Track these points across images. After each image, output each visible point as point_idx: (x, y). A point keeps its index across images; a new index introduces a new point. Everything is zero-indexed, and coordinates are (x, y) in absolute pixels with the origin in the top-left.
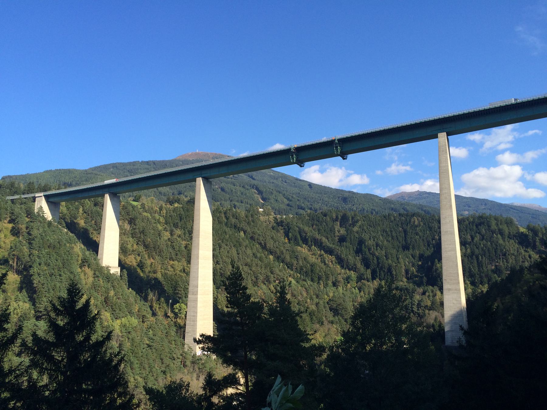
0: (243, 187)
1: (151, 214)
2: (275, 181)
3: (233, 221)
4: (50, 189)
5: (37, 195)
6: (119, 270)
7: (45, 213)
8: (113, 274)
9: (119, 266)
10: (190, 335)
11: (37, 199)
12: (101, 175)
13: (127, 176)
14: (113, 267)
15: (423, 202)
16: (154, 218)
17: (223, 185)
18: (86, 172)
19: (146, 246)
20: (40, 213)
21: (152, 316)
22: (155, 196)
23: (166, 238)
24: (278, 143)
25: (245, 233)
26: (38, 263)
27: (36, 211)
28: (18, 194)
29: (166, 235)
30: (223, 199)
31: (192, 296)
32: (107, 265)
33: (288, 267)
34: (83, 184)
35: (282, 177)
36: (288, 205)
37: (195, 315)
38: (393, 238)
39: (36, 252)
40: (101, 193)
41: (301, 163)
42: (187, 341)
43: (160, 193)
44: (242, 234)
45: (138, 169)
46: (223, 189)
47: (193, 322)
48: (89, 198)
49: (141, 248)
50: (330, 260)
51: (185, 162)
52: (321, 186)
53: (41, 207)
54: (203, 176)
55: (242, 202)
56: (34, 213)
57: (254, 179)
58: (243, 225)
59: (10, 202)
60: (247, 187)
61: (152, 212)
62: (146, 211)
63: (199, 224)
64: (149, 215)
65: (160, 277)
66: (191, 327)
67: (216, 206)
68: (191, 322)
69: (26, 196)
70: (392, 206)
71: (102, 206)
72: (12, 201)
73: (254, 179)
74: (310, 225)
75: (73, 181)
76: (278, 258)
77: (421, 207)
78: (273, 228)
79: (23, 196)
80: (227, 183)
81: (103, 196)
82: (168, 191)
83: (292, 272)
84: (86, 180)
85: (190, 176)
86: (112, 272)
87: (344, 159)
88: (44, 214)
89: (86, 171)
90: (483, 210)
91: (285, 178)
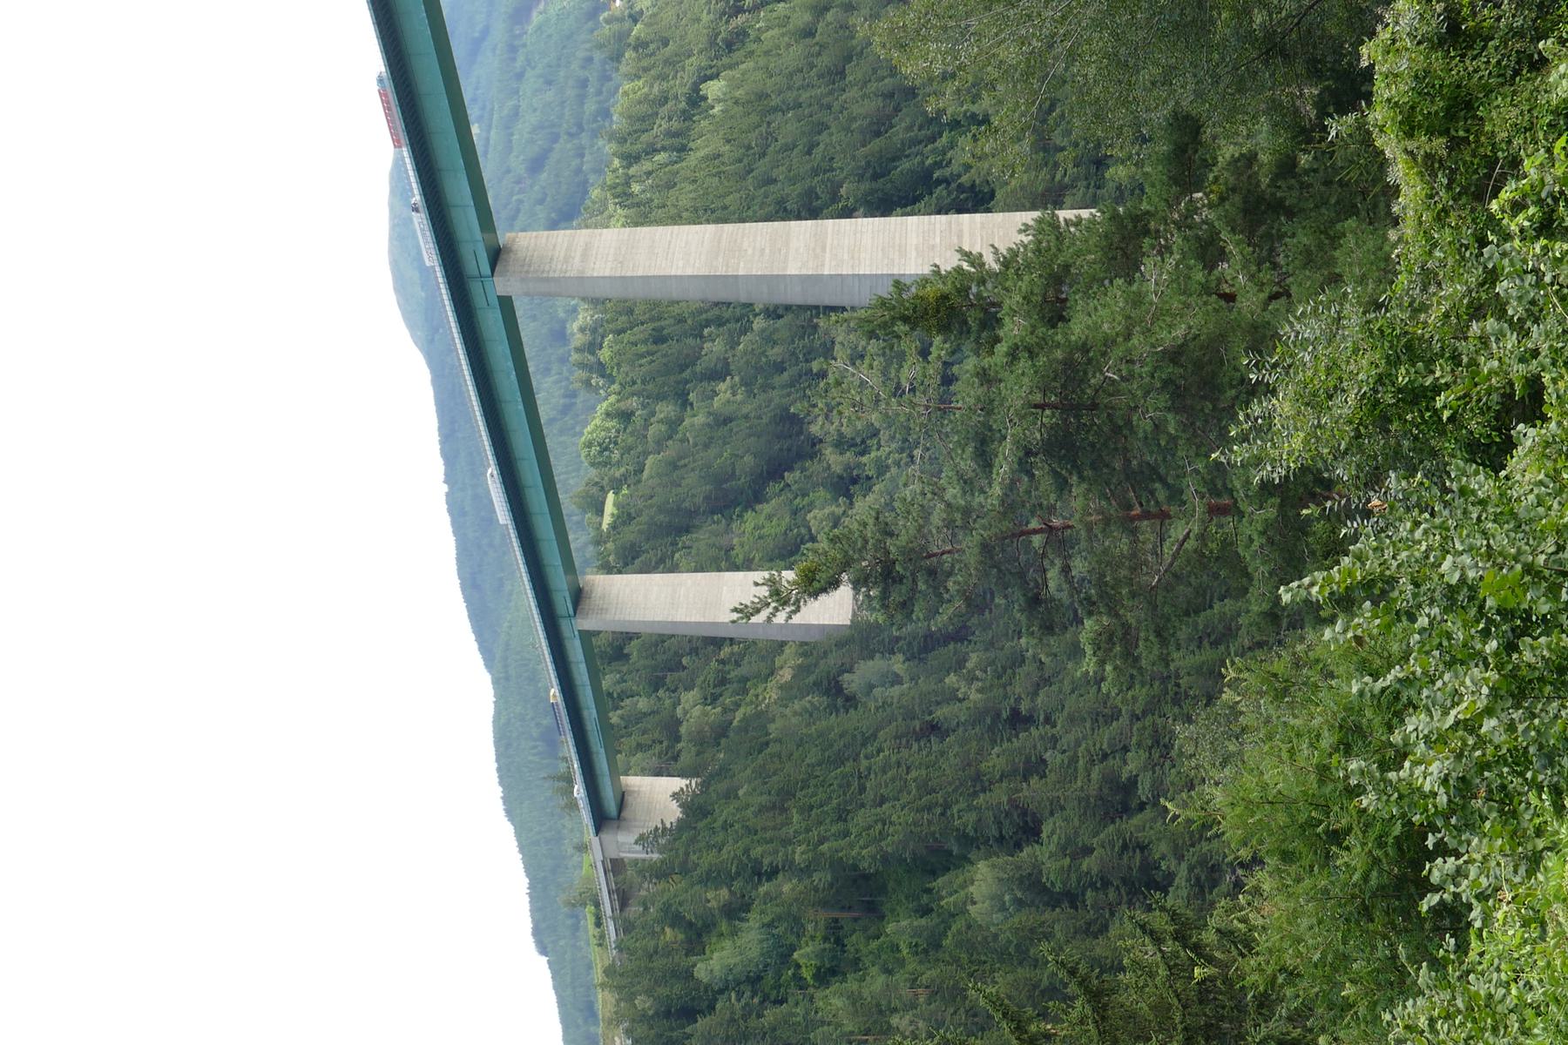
0: (520, 76)
1: (646, 454)
3: (661, 125)
12: (510, 627)
17: (518, 164)
20: (662, 841)
21: (1175, 114)
22: (578, 429)
26: (1041, 331)
27: (656, 856)
29: (725, 394)
30: (575, 162)
39: (799, 854)
40: (577, 643)
43: (566, 410)
44: (713, 89)
46: (536, 165)
54: (486, 269)
57: (486, 32)
58: (680, 85)
60: (519, 64)
61: (640, 449)
63: (680, 279)
65: (724, 893)
73: (486, 32)
75: (538, 725)
80: (509, 148)
82: (556, 382)
89: (496, 682)
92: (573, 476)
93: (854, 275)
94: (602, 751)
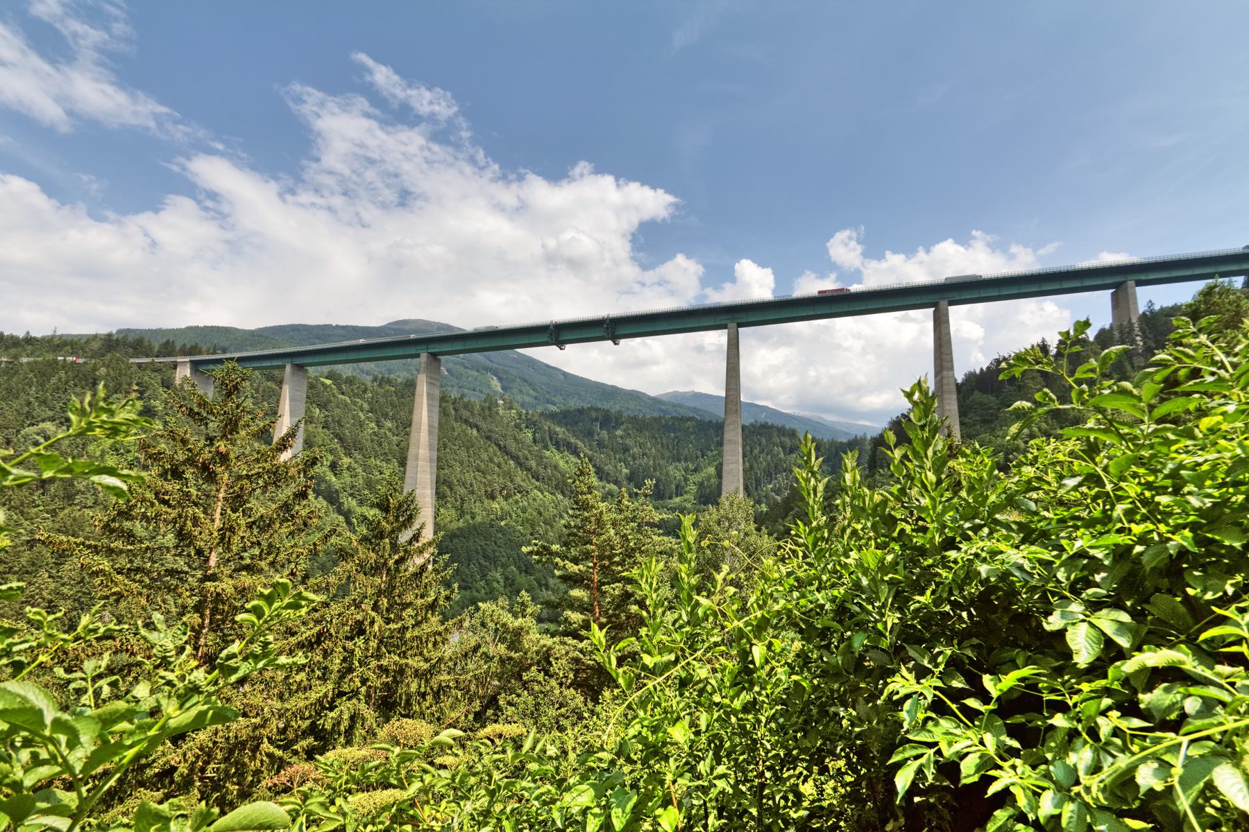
2: (519, 366)
4: (200, 353)
5: (179, 360)
13: (314, 344)
15: (698, 405)
16: (355, 404)
18: (252, 334)
19: (341, 440)
23: (370, 431)
24: (836, 231)
25: (478, 431)
28: (147, 356)
33: (533, 477)
34: (247, 350)
36: (536, 398)
38: (662, 446)
40: (280, 363)
41: (560, 344)
45: (329, 335)
48: (424, 347)
49: (336, 444)
54: (430, 351)
55: (474, 390)
58: (476, 420)
59: (135, 368)
62: (343, 393)
64: (347, 399)
67: (729, 772)
69: (161, 360)
70: (663, 407)
72: (139, 365)
73: (491, 361)
76: (520, 464)
77: (695, 410)
78: (517, 426)
79: (157, 360)
80: (455, 363)
81: (283, 367)
83: (538, 483)
84: (251, 345)
85: (412, 351)
87: (615, 344)
90: (762, 418)
91: (532, 363)
92: (346, 370)
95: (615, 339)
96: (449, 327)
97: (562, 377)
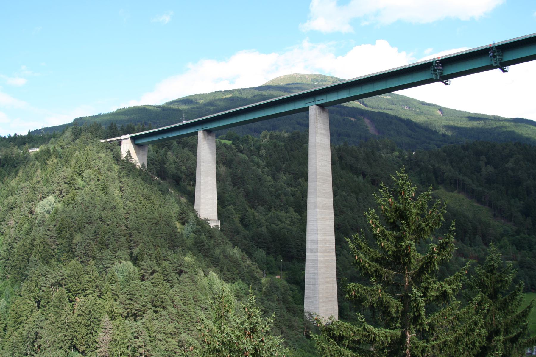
5: (122, 137)
6: (218, 223)
7: (132, 157)
8: (214, 228)
9: (218, 219)
10: (311, 301)
11: (123, 142)
14: (212, 220)
31: (311, 254)
32: (206, 217)
35: (403, 101)
37: (316, 277)
42: (307, 308)
47: (313, 286)
50: (39, 190)
51: (297, 86)
52: (455, 110)
53: (129, 152)
54: (318, 103)
56: (444, 135)
62: (241, 152)
66: (311, 291)
68: (311, 286)
71: (194, 148)
74: (447, 162)
86: (212, 225)
87: (504, 71)
88: (132, 159)
91: (407, 101)
93: (317, 219)
94: (157, 139)
95: (503, 66)
96: (324, 79)
97: (440, 113)
